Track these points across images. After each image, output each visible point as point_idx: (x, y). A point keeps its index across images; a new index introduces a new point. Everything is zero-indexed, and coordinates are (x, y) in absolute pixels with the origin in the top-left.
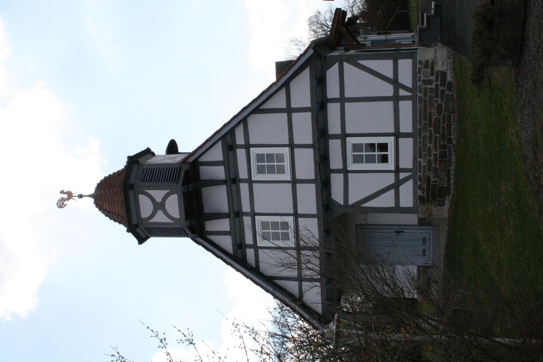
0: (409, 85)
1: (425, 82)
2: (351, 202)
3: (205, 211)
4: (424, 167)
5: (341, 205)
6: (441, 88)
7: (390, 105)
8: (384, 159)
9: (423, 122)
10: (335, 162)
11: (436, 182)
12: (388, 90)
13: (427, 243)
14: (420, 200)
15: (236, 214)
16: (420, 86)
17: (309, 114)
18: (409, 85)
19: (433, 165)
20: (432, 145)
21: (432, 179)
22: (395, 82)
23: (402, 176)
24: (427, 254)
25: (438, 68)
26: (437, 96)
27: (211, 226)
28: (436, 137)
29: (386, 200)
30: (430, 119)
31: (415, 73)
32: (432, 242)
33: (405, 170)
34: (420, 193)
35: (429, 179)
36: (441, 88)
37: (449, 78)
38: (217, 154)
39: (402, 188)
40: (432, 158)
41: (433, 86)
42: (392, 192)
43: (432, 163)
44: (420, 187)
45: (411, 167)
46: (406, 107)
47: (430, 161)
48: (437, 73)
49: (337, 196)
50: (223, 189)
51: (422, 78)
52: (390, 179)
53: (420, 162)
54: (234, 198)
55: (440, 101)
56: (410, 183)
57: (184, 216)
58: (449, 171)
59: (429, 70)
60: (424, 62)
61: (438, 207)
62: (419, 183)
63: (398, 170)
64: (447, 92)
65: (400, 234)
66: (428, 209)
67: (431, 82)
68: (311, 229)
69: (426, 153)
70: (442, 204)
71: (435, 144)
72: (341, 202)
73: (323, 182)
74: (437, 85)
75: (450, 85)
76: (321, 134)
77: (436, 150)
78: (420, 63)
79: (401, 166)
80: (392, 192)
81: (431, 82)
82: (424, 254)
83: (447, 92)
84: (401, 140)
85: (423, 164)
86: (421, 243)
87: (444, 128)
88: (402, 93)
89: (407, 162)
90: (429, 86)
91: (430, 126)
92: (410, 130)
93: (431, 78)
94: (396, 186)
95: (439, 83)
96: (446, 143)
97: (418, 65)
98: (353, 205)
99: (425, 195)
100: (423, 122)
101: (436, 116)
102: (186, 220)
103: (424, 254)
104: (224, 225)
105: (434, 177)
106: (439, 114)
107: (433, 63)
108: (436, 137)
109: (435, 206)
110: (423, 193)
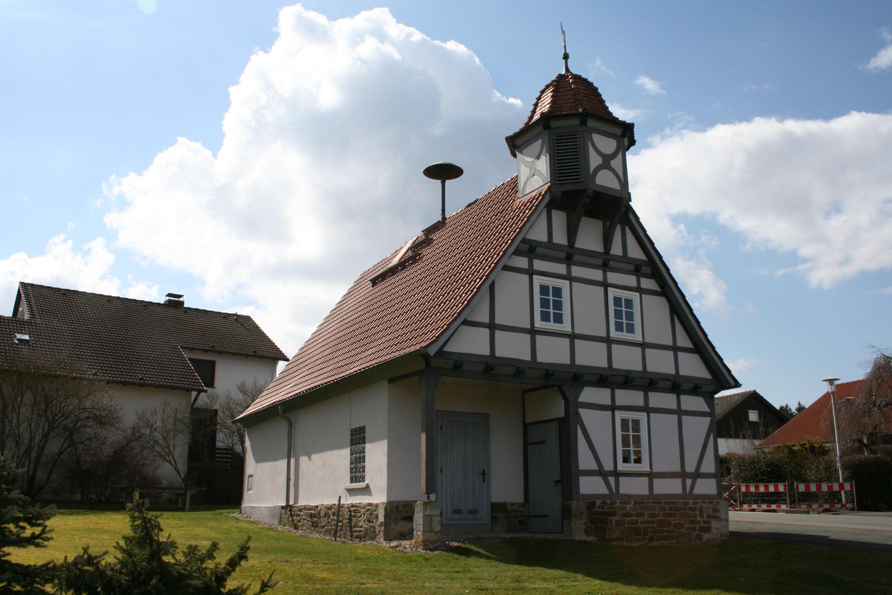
0: (697, 491)
1: (701, 509)
2: (582, 411)
3: (583, 218)
4: (625, 508)
5: (578, 397)
6: (697, 526)
7: (677, 468)
8: (626, 460)
9: (667, 507)
10: (625, 397)
11: (611, 524)
12: (690, 468)
13: (471, 516)
14: (591, 502)
15: (570, 255)
16: (697, 503)
17: (673, 372)
18: (697, 491)
19: (628, 519)
20: (646, 518)
21: (614, 519)
22: (697, 475)
23: (612, 480)
24: (456, 515)
25: (714, 524)
26: (691, 522)
27: (559, 218)
28: (653, 522)
29: (585, 460)
30: (669, 515)
31: (704, 497)
32: (472, 522)
33: (693, 486)
34: (598, 502)
35: (613, 514)
36: (697, 526)
37: (706, 536)
38: (635, 252)
39: (599, 479)
40: (634, 518)
41: (699, 518)
42: (596, 468)
43: (630, 518)
44: (604, 503)
45: (621, 492)
46: (673, 487)
47: (631, 515)
48: (709, 523)
49: (589, 394)
50: (599, 248)
51: (705, 505)
52: (608, 466)
53: (629, 503)
54: (588, 258)
55: (686, 526)
56: (605, 491)
57: (597, 190)
58: (622, 540)
59: (711, 513)
60: (718, 507)
61: (583, 527)
62: (608, 502)
63: (617, 474)
64: (694, 534)
65: (482, 477)
66: (582, 513)
67: (701, 516)
68: (554, 352)
69: (639, 511)
70: (587, 533)
71: (647, 522)
72: (582, 399)
73: (607, 378)
74: (699, 522)
75: (699, 537)
76: (648, 382)
77: (642, 523)
78: (717, 503)
79: (622, 479)
80: (596, 468)
81: (701, 516)
82: (456, 512)
83: (694, 534)
84: (645, 480)
85: (628, 506)
86: (471, 508)
87: (662, 532)
88: (689, 482)
89: (628, 487)
90: (698, 513)
91: (664, 515)
92: (657, 491)
93: (705, 515)
94: (601, 472)
95: (702, 525)
96: (650, 535)
97: (715, 501)
98: (578, 413)
99: (597, 509)
100: (667, 507)
101: (673, 522)
102: (594, 191)
103: (456, 512)
104: (560, 238)
105: (616, 521)
106: (675, 526)
107: (717, 518)
108: (653, 522)
109: (585, 523)
110: (599, 507)
